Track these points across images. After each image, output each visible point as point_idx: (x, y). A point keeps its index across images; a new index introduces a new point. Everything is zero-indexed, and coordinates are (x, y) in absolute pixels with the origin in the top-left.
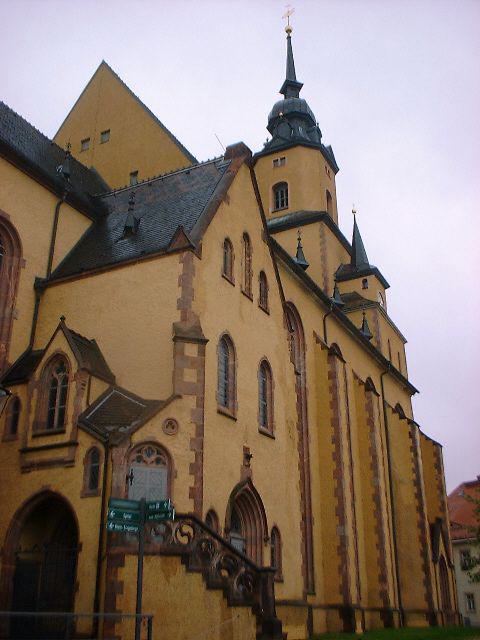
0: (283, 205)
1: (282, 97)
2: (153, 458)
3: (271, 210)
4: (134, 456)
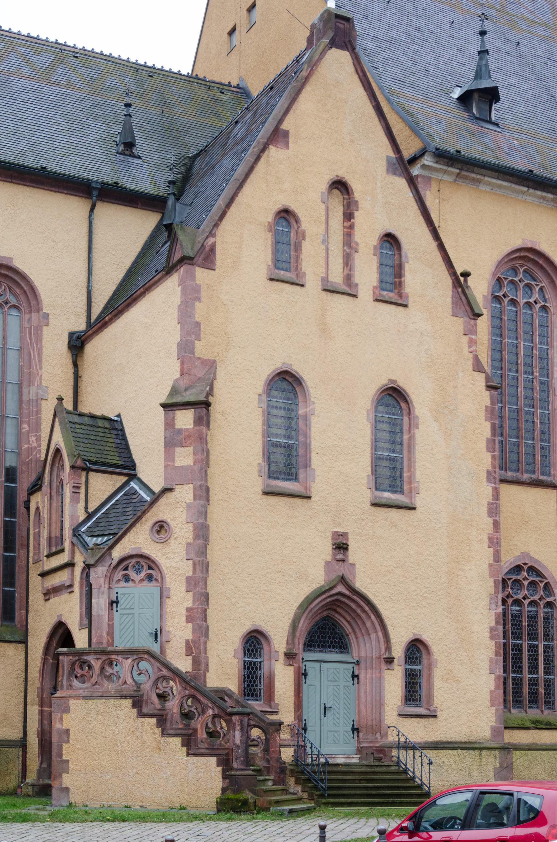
2: (143, 574)
4: (119, 574)
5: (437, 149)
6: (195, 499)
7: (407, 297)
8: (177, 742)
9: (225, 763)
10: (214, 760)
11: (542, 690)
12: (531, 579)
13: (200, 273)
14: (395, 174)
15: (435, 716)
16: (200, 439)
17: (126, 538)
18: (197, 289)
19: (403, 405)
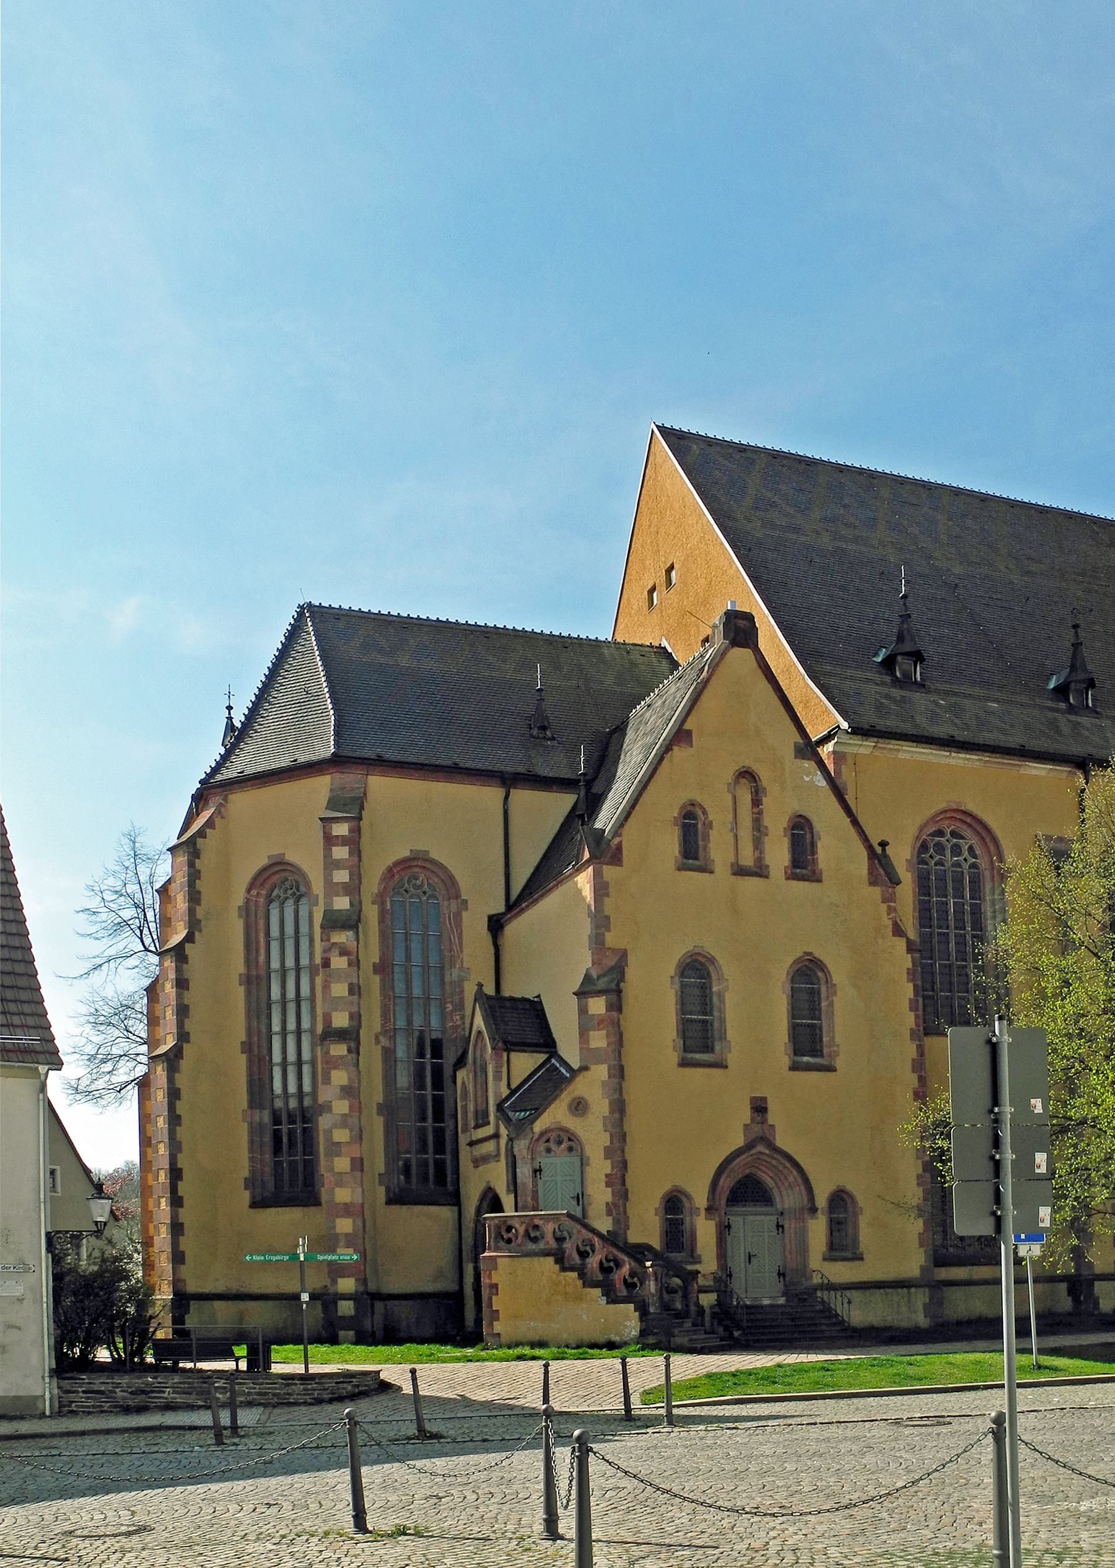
15: (862, 1259)
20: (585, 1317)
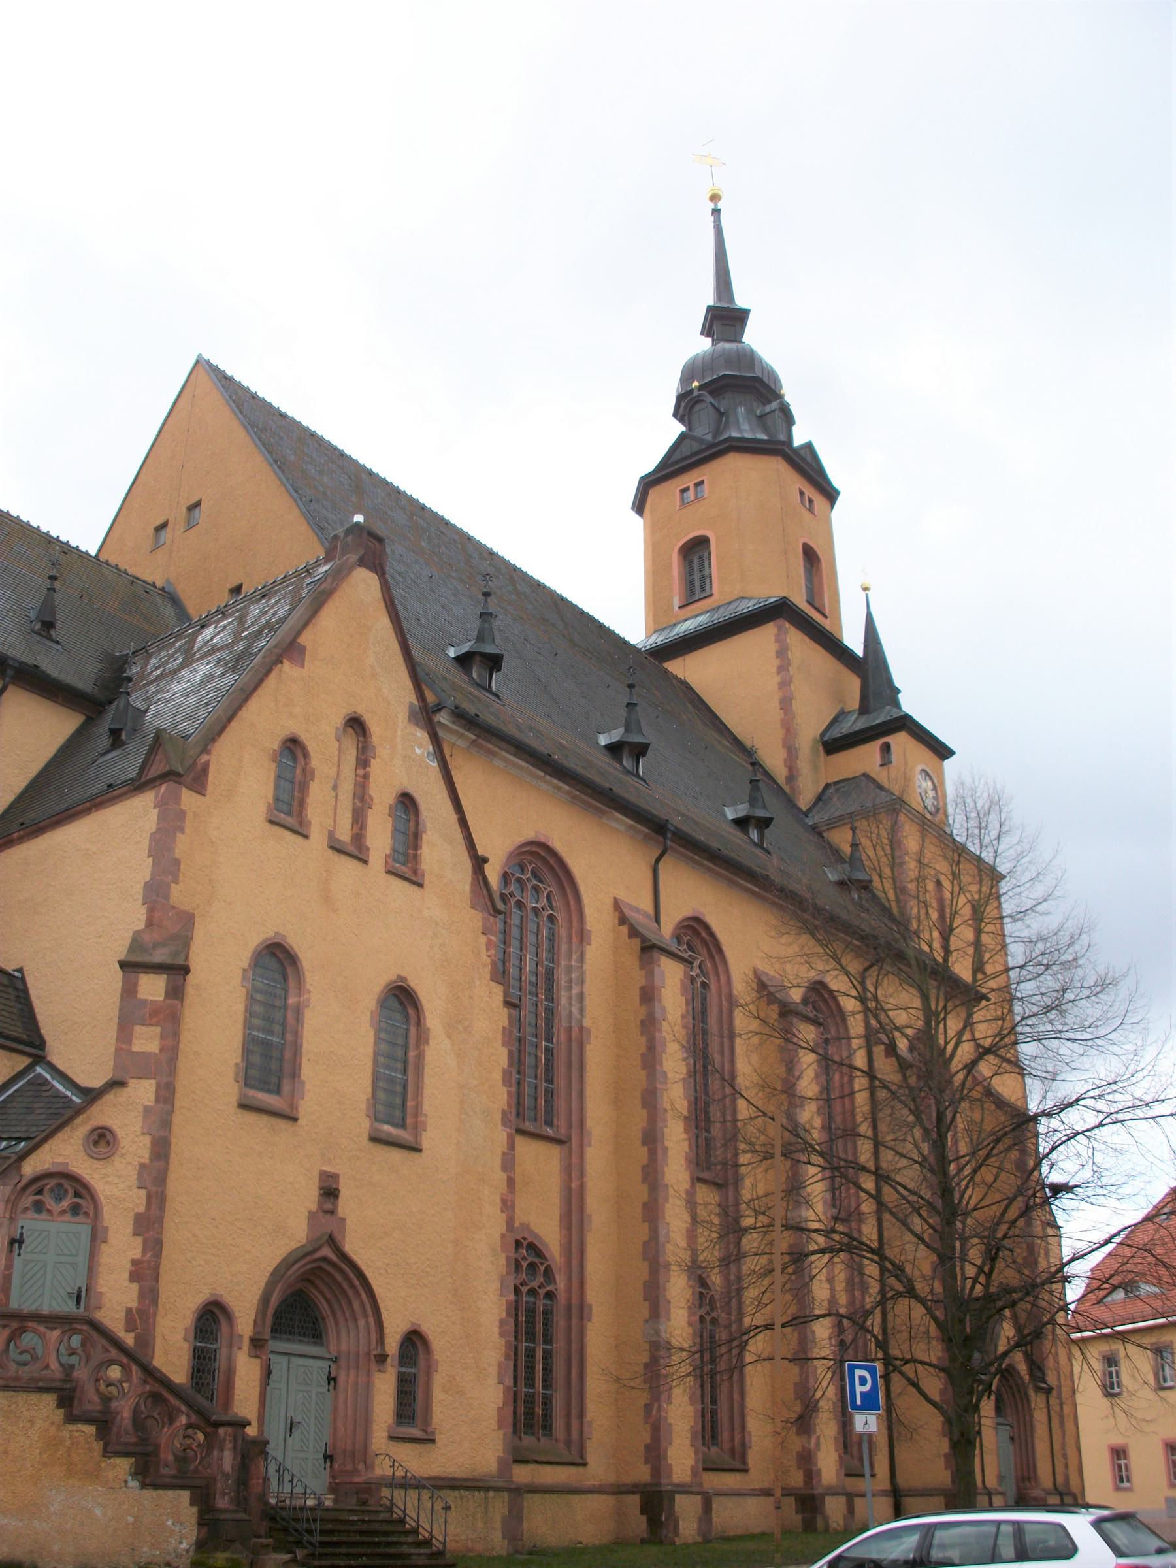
0: (703, 589)
1: (706, 344)
2: (65, 1204)
3: (676, 603)
4: (28, 1200)
5: (456, 707)
6: (157, 1100)
7: (423, 875)
8: (124, 1465)
9: (203, 1498)
10: (185, 1495)
11: (539, 1410)
12: (530, 1259)
13: (188, 798)
14: (417, 725)
16: (170, 1016)
17: (47, 1146)
18: (182, 815)
19: (411, 1011)
20: (98, 1512)
